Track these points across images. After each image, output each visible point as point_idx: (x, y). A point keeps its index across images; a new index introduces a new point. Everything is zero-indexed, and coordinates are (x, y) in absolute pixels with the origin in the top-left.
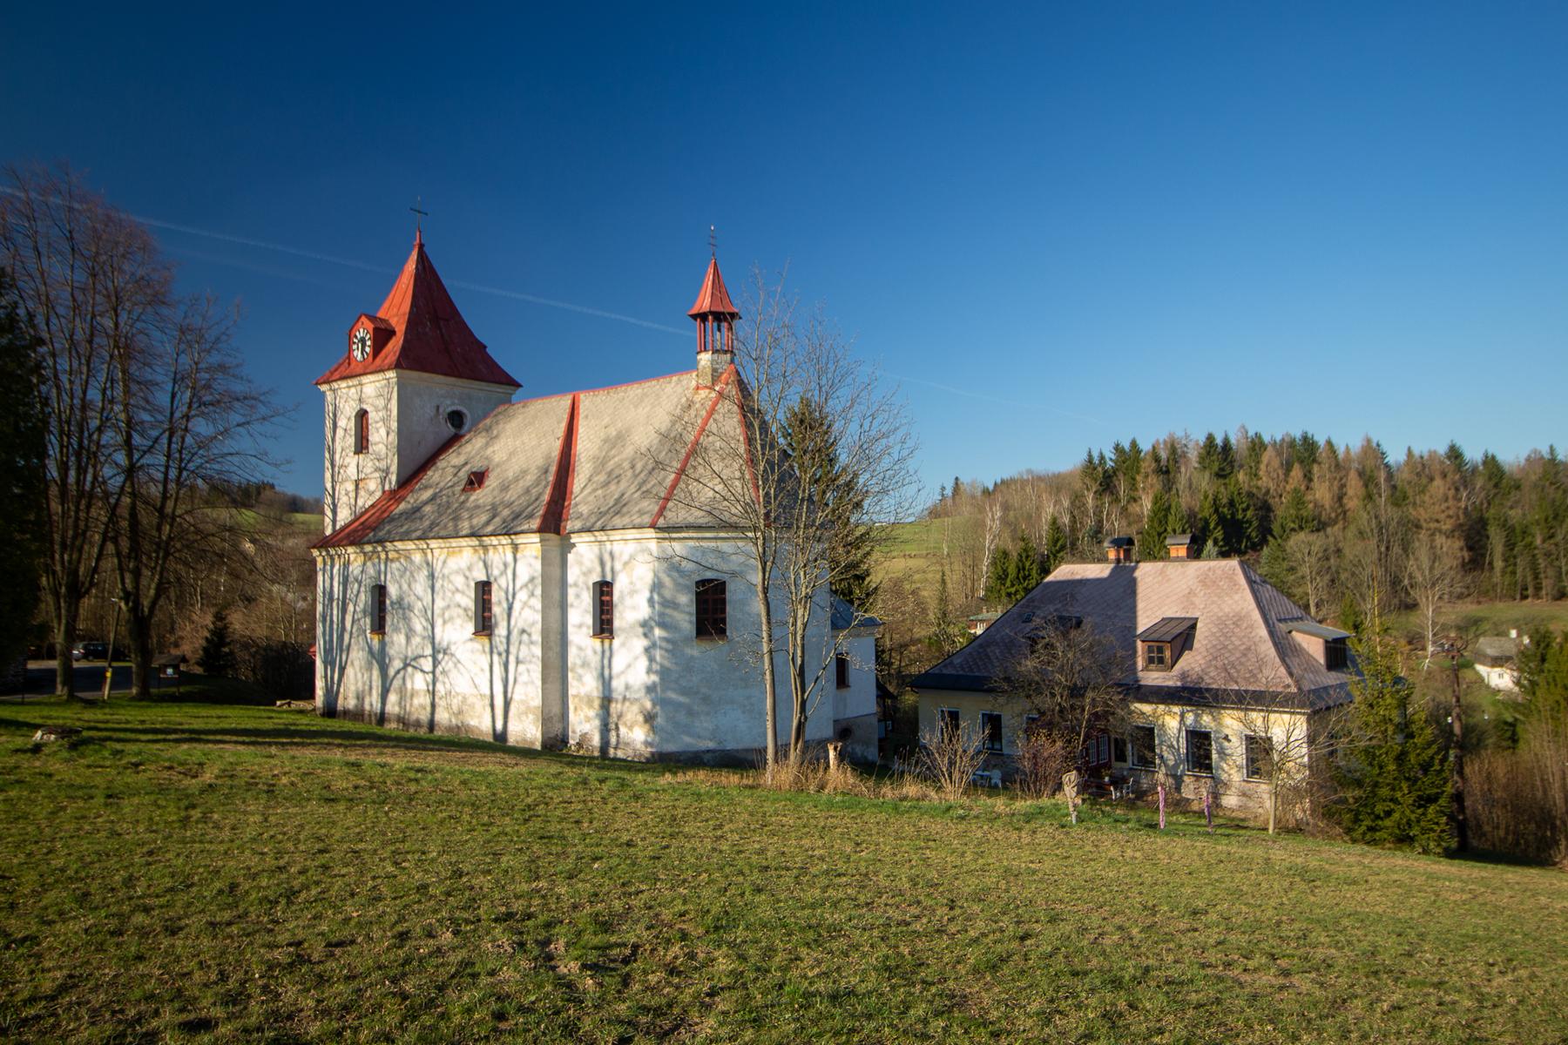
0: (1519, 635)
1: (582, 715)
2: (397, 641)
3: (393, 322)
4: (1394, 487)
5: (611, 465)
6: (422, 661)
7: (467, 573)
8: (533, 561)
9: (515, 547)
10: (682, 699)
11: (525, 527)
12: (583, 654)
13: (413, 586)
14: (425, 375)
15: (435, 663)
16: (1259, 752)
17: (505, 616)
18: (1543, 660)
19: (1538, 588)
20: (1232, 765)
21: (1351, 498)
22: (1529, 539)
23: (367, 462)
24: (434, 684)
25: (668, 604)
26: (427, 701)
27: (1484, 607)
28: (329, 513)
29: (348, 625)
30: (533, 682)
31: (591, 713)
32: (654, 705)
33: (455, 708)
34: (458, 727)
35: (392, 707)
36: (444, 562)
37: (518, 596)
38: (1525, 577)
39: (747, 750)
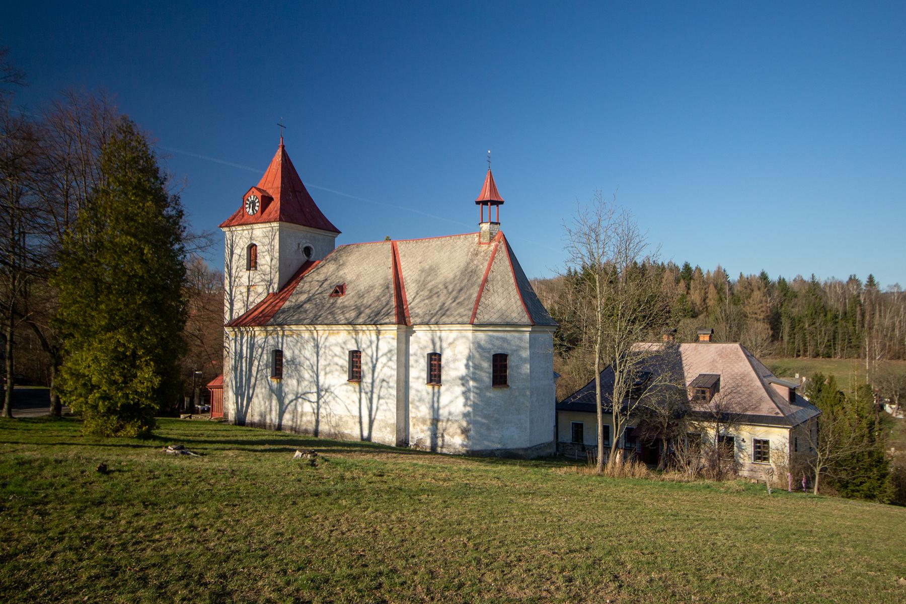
0: (801, 377)
1: (418, 429)
2: (291, 384)
3: (271, 192)
4: (733, 294)
5: (430, 286)
6: (309, 396)
7: (343, 346)
8: (391, 341)
9: (378, 332)
10: (484, 421)
11: (387, 321)
12: (419, 394)
13: (303, 352)
14: (293, 225)
15: (319, 397)
16: (761, 450)
17: (371, 371)
18: (820, 391)
19: (805, 351)
20: (746, 456)
21: (710, 300)
22: (801, 325)
23: (257, 277)
24: (318, 409)
25: (476, 367)
26: (314, 419)
27: (778, 360)
28: (227, 304)
29: (254, 373)
30: (390, 410)
31: (425, 428)
32: (469, 423)
33: (333, 423)
34: (335, 434)
35: (287, 420)
36: (326, 338)
37: (380, 360)
38: (799, 345)
39: (517, 449)
